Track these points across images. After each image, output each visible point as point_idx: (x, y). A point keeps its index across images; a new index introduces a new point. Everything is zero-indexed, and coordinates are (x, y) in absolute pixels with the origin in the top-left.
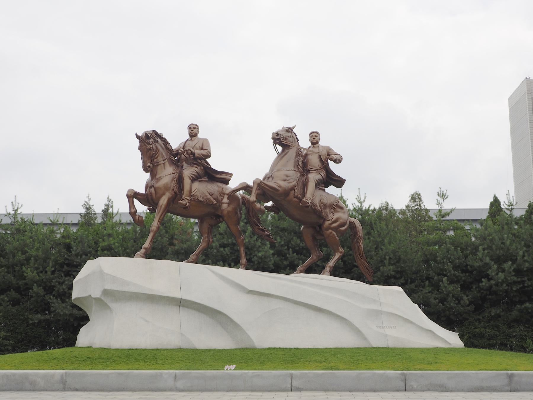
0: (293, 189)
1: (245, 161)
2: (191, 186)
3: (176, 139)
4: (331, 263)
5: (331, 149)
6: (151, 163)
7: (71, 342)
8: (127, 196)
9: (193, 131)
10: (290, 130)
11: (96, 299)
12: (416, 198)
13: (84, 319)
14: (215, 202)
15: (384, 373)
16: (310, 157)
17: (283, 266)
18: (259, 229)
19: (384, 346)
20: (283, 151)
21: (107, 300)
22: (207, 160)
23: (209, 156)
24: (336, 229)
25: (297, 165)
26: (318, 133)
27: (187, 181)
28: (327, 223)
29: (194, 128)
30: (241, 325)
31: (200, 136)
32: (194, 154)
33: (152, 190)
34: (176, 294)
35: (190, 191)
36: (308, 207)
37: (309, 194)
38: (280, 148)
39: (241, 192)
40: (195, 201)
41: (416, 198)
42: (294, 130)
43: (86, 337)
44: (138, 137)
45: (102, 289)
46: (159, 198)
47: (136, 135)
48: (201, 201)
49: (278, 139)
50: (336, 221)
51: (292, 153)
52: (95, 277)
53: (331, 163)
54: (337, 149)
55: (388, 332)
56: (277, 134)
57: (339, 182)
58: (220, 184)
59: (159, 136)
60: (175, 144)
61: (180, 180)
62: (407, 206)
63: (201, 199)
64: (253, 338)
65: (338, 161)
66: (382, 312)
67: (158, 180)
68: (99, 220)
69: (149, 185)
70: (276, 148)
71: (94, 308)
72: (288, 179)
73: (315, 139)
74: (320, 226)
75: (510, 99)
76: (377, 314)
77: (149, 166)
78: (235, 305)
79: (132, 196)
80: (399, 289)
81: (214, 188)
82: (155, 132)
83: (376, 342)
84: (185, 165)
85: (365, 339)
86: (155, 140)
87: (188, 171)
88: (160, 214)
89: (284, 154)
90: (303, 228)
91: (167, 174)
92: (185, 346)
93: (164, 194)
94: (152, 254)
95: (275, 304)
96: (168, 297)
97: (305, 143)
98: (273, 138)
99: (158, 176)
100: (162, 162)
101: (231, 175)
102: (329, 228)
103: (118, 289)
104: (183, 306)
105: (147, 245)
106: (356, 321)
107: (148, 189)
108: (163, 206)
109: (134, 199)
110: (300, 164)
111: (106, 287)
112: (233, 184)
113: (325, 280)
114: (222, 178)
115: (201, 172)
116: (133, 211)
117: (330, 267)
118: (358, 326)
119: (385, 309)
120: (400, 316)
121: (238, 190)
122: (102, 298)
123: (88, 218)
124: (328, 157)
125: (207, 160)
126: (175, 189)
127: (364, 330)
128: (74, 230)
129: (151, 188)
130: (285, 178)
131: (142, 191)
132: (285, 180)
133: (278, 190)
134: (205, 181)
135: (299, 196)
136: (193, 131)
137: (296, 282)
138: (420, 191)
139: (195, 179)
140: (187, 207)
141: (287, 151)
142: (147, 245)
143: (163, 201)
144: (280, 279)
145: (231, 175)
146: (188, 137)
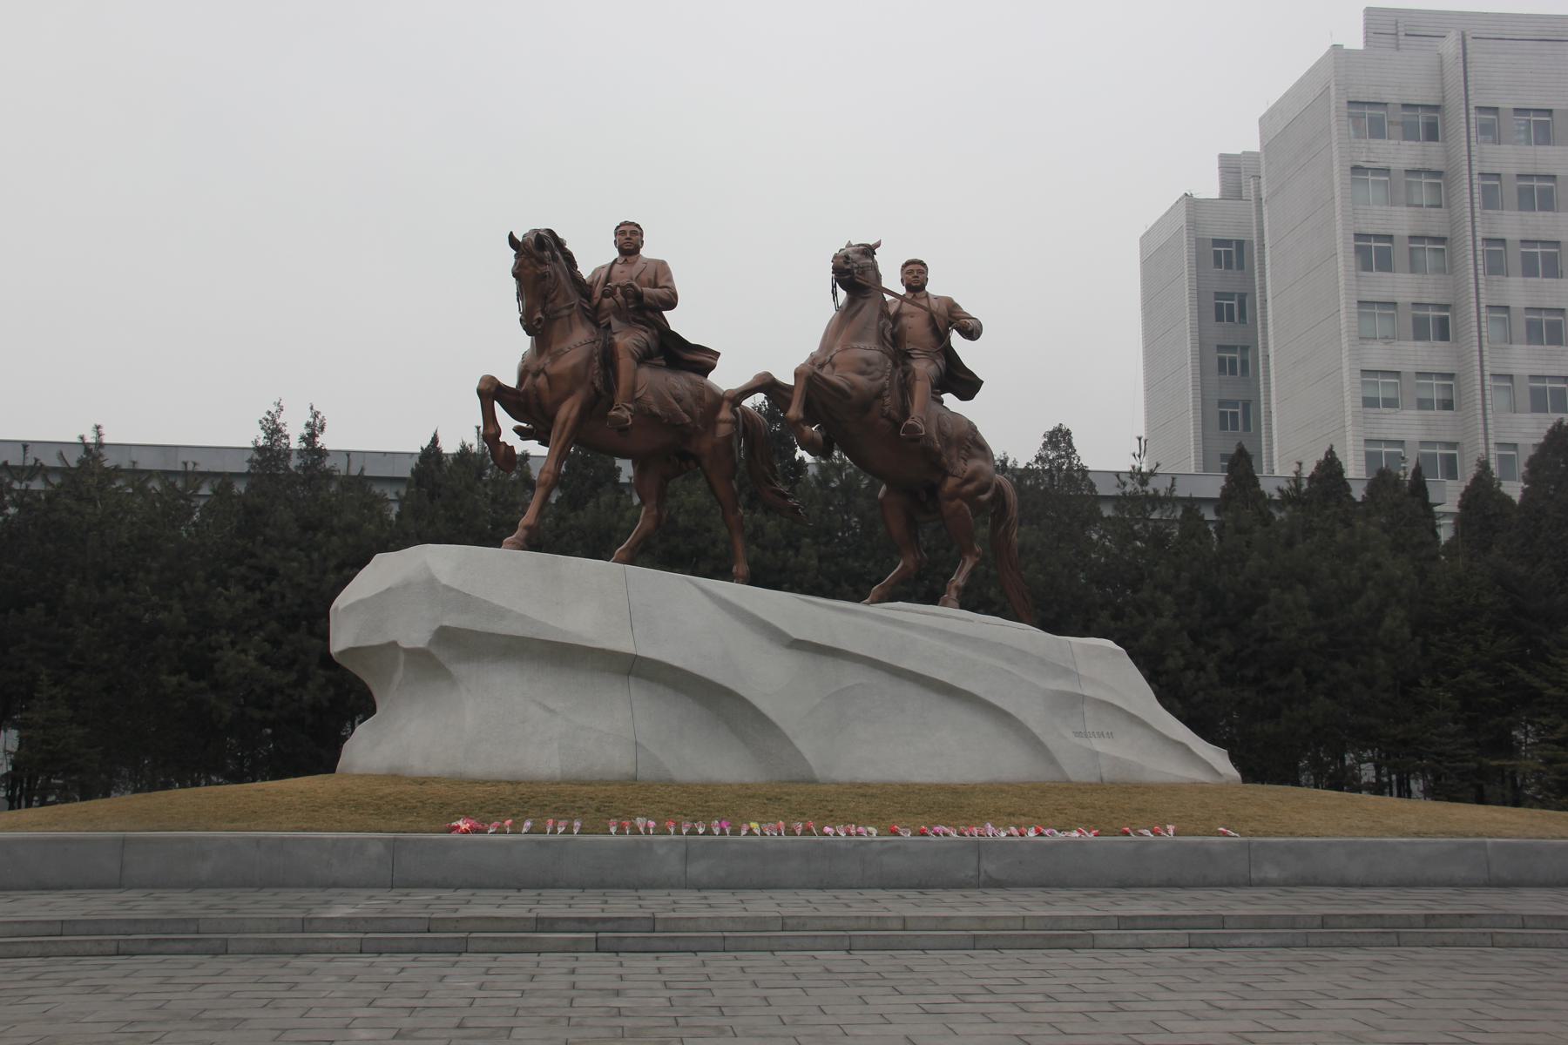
0: (879, 395)
1: (756, 325)
2: (635, 375)
3: (593, 255)
4: (959, 579)
5: (956, 306)
6: (543, 312)
7: (324, 758)
8: (480, 392)
9: (629, 239)
10: (869, 251)
11: (412, 652)
12: (1059, 439)
13: (365, 707)
14: (688, 419)
15: (1201, 843)
16: (905, 321)
17: (843, 580)
18: (774, 492)
19: (1094, 779)
20: (851, 301)
21: (442, 655)
22: (665, 313)
23: (671, 303)
24: (970, 498)
25: (881, 338)
26: (924, 265)
27: (625, 363)
28: (951, 482)
29: (633, 233)
30: (779, 723)
31: (645, 252)
32: (639, 297)
33: (542, 380)
34: (625, 645)
35: (634, 389)
36: (917, 440)
37: (916, 411)
38: (842, 295)
39: (759, 398)
40: (646, 417)
41: (1059, 439)
42: (879, 256)
43: (368, 750)
44: (513, 241)
45: (436, 627)
46: (558, 403)
47: (511, 237)
48: (656, 416)
49: (849, 272)
50: (969, 480)
51: (869, 310)
52: (386, 597)
53: (956, 339)
54: (969, 306)
55: (1098, 745)
56: (847, 257)
57: (968, 386)
58: (694, 376)
59: (560, 244)
60: (586, 270)
61: (608, 358)
62: (1039, 459)
63: (656, 410)
64: (808, 756)
65: (972, 332)
66: (1083, 699)
67: (556, 357)
68: (294, 462)
69: (533, 367)
70: (835, 294)
71: (399, 675)
72: (870, 369)
73: (915, 274)
74: (933, 490)
75: (1145, 239)
76: (1074, 702)
77: (539, 320)
78: (764, 677)
79: (491, 392)
80: (1109, 644)
81: (680, 382)
82: (551, 232)
83: (1076, 770)
84: (615, 323)
85: (1051, 760)
86: (553, 253)
87: (628, 339)
88: (561, 442)
89: (855, 309)
90: (887, 493)
91: (578, 342)
92: (645, 773)
93: (570, 393)
94: (534, 543)
95: (852, 676)
96: (603, 650)
97: (892, 281)
98: (836, 270)
99: (555, 348)
100: (566, 312)
101: (718, 354)
102: (954, 495)
103: (478, 628)
104: (638, 675)
105: (528, 518)
106: (1032, 716)
107: (529, 378)
108: (569, 424)
109: (497, 405)
110: (888, 336)
111: (446, 623)
112: (724, 379)
113: (949, 618)
114: (700, 360)
115: (654, 344)
116: (492, 431)
117: (957, 588)
118: (1037, 731)
119: (1088, 692)
120: (1120, 709)
121: (748, 392)
122: (434, 651)
123: (269, 456)
124: (953, 320)
125: (665, 313)
126: (597, 384)
127: (1049, 740)
128: (240, 487)
129: (536, 375)
130: (864, 366)
131: (510, 380)
132: (862, 373)
133: (849, 397)
134: (660, 366)
135: (895, 414)
136: (629, 239)
137: (893, 622)
138: (1067, 426)
139: (644, 358)
140: (626, 429)
141: (861, 302)
142: (528, 518)
143: (568, 411)
144: (855, 613)
145: (718, 354)
146: (615, 254)
